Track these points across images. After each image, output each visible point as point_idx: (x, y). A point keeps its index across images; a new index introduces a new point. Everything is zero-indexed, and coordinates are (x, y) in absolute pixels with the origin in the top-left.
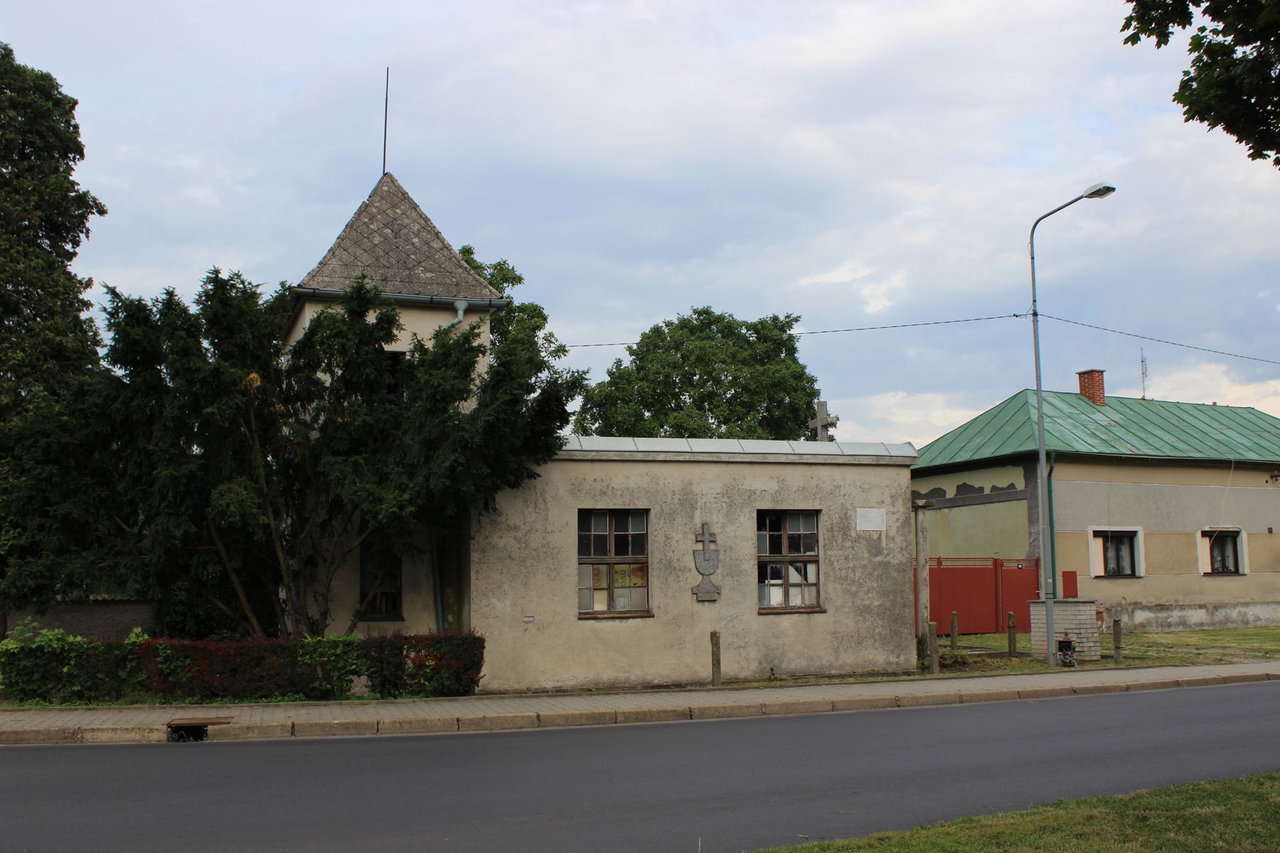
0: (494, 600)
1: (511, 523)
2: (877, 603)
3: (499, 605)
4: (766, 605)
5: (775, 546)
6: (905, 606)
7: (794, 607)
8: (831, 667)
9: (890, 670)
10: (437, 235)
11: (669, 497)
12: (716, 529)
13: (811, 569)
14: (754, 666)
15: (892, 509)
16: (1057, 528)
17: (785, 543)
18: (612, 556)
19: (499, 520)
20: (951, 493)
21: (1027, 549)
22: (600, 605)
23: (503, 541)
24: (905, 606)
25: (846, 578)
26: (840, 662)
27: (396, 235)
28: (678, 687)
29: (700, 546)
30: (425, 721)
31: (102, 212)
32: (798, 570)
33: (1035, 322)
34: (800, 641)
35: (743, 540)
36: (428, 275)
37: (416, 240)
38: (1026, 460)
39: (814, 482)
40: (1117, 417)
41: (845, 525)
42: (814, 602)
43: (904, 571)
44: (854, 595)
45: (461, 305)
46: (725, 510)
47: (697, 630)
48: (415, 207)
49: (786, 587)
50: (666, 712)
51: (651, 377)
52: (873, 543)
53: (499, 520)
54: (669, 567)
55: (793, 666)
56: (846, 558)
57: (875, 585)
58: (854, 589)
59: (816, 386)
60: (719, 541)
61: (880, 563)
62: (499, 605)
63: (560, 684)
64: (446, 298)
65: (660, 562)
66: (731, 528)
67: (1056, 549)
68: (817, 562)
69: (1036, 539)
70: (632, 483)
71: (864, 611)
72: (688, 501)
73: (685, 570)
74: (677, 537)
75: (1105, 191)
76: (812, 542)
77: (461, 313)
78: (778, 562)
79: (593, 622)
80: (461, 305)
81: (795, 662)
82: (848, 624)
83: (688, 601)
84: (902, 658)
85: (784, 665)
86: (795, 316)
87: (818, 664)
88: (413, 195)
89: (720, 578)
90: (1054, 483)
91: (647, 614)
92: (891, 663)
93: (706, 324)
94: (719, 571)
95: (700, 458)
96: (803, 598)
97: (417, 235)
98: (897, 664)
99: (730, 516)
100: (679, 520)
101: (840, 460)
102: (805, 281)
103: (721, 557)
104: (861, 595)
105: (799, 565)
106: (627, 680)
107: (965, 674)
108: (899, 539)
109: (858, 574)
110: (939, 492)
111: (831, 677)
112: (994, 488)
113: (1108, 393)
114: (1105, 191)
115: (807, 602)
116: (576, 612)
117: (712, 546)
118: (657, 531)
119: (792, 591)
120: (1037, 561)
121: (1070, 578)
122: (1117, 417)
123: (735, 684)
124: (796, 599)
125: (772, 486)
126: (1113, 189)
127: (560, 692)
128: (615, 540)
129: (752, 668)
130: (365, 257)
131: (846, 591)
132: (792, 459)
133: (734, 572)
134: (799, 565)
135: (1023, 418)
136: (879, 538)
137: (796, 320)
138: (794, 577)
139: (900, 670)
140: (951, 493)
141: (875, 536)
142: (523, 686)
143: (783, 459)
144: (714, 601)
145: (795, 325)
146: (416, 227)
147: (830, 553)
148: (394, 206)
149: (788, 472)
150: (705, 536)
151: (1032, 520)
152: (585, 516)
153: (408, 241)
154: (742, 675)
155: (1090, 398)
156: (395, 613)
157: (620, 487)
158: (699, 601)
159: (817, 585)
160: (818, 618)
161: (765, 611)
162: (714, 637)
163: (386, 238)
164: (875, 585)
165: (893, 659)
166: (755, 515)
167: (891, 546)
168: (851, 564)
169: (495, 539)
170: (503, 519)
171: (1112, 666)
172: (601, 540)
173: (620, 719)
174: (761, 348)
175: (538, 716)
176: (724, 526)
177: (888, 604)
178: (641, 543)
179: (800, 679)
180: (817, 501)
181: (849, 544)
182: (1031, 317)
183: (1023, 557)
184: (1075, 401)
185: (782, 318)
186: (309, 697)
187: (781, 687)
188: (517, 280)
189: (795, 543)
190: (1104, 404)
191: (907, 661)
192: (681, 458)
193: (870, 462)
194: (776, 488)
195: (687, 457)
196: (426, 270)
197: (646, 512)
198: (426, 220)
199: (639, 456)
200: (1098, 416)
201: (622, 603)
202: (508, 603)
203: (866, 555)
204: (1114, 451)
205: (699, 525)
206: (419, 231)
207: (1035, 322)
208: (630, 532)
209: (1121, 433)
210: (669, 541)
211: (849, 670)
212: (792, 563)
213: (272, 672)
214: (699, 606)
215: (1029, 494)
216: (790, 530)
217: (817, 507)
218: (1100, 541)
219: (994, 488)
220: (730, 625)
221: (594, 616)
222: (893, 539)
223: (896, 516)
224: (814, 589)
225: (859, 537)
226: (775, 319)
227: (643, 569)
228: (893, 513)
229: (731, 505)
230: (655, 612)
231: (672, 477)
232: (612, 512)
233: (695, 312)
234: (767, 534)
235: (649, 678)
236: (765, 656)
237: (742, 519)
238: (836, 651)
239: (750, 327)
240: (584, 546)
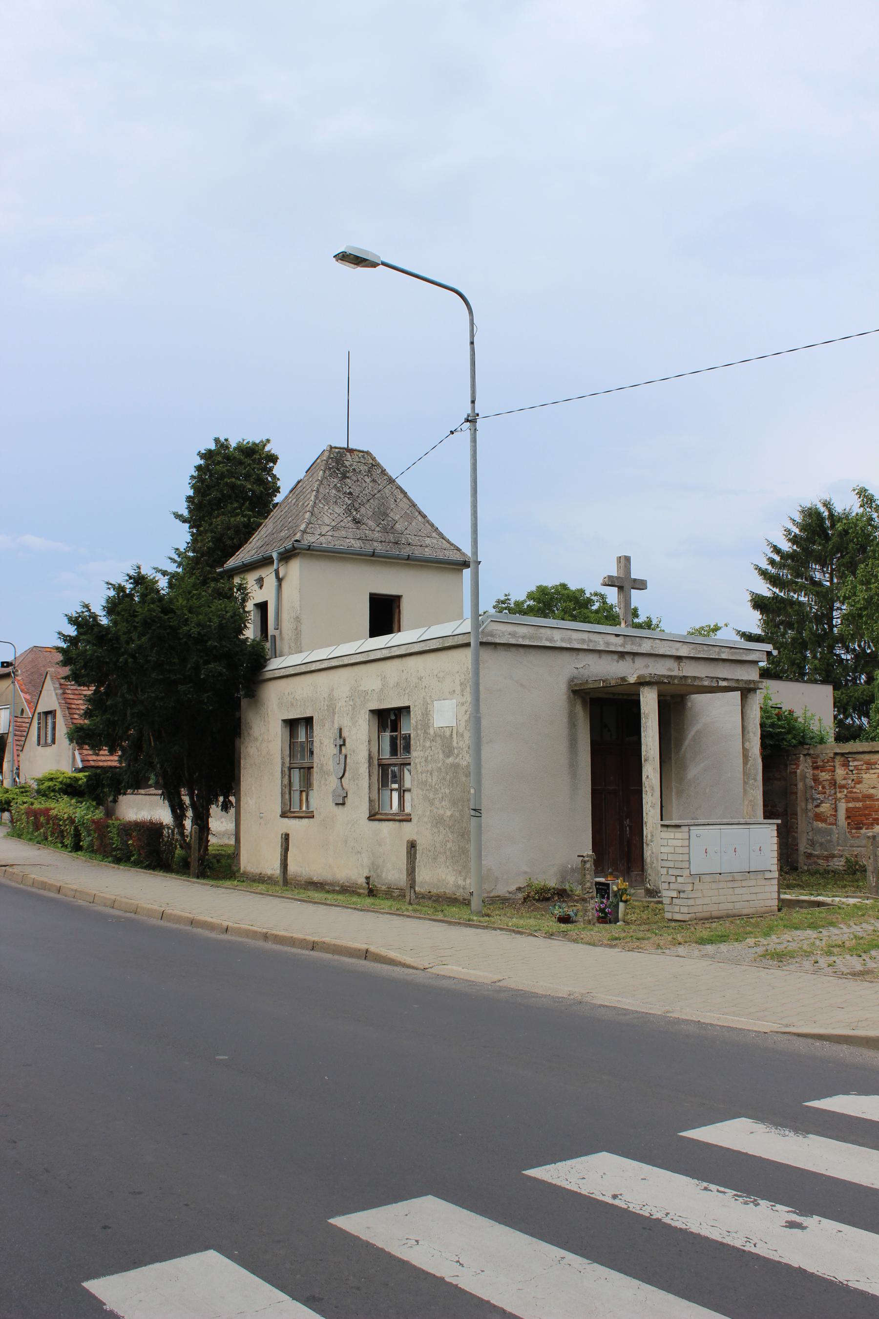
2: (449, 813)
92: (458, 887)
123: (317, 888)
141: (448, 734)
167: (461, 744)
168: (429, 768)
177: (457, 814)
197: (409, 707)
203: (441, 756)
228: (463, 704)
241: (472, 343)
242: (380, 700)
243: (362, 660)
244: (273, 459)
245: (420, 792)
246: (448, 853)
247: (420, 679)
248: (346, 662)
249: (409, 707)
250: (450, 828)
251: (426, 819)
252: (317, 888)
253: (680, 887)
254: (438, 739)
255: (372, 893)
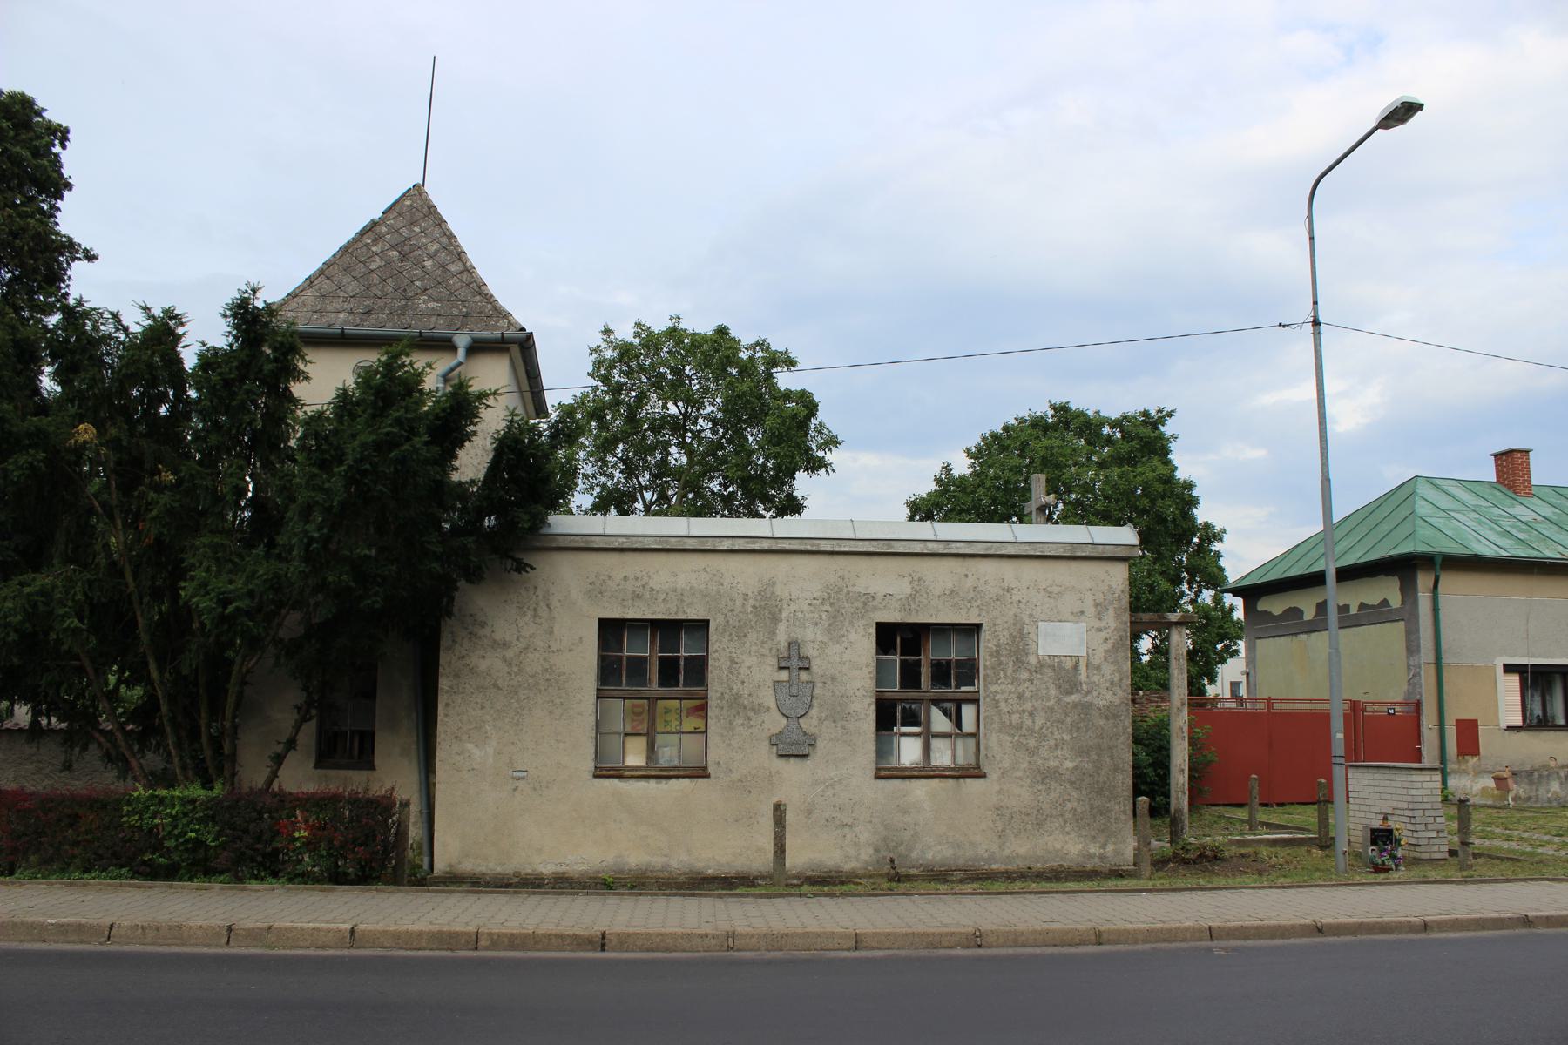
0: (469, 746)
1: (498, 636)
2: (1069, 765)
3: (477, 753)
4: (893, 762)
5: (910, 676)
6: (1116, 769)
7: (937, 768)
8: (992, 859)
9: (1089, 867)
10: (460, 255)
11: (739, 603)
12: (810, 651)
13: (968, 712)
14: (866, 854)
15: (1097, 624)
16: (1447, 660)
17: (926, 673)
18: (654, 686)
19: (481, 632)
20: (1309, 614)
21: (1405, 687)
22: (635, 756)
23: (488, 663)
24: (1116, 769)
25: (1020, 727)
26: (1007, 852)
27: (404, 257)
28: (698, 884)
29: (784, 675)
30: (180, 927)
31: (90, 257)
32: (945, 712)
33: (1317, 335)
34: (941, 821)
35: (854, 666)
36: (431, 305)
37: (428, 263)
38: (1404, 567)
39: (970, 583)
40: (1548, 511)
41: (1019, 645)
42: (972, 761)
43: (1116, 717)
44: (1032, 752)
45: (462, 341)
46: (825, 623)
47: (798, 794)
48: (441, 222)
49: (927, 737)
50: (561, 936)
51: (988, 483)
52: (1066, 675)
53: (481, 632)
54: (736, 704)
55: (930, 856)
56: (1020, 697)
57: (1066, 737)
58: (1032, 742)
59: (1195, 493)
60: (815, 669)
61: (1075, 705)
62: (477, 753)
63: (564, 869)
64: (442, 331)
65: (722, 697)
66: (834, 650)
67: (1446, 688)
68: (976, 701)
69: (1417, 675)
70: (681, 583)
71: (1047, 776)
72: (768, 610)
73: (759, 709)
74: (749, 661)
75: (1403, 112)
76: (968, 671)
77: (461, 352)
78: (914, 701)
79: (616, 781)
80: (462, 341)
81: (933, 850)
82: (1021, 794)
83: (764, 757)
84: (1110, 848)
85: (914, 854)
86: (1168, 409)
87: (970, 853)
88: (443, 211)
89: (815, 722)
90: (1442, 598)
91: (701, 772)
92: (1091, 856)
93: (1066, 419)
94: (813, 712)
95: (787, 546)
96: (954, 756)
97: (431, 257)
98: (1102, 857)
99: (834, 629)
100: (753, 636)
101: (1012, 550)
102: (1268, 399)
103: (817, 691)
104: (1044, 752)
105: (947, 705)
106: (665, 868)
107: (1222, 882)
108: (1108, 669)
109: (1040, 721)
110: (1295, 612)
111: (991, 876)
112: (1362, 606)
113: (1536, 479)
114: (1403, 112)
115: (961, 761)
116: (591, 765)
117: (804, 676)
118: (720, 649)
119: (936, 744)
120: (1418, 704)
121: (1468, 734)
122: (1548, 511)
123: (825, 882)
124: (942, 755)
125: (903, 588)
126: (1420, 107)
127: (563, 884)
128: (656, 662)
129: (864, 856)
130: (353, 287)
131: (1018, 746)
132: (932, 547)
133: (839, 713)
134: (947, 705)
135: (1403, 512)
136: (1076, 667)
137: (1170, 415)
138: (940, 722)
139: (1106, 867)
140: (1309, 614)
141: (1069, 664)
142: (507, 868)
143: (918, 548)
144: (805, 756)
145: (1169, 421)
146: (434, 247)
147: (993, 688)
148: (413, 223)
149: (927, 567)
150: (794, 660)
151: (1412, 648)
152: (611, 630)
153: (418, 264)
154: (847, 867)
155: (1509, 488)
156: (364, 758)
157: (666, 589)
158: (781, 756)
159: (975, 735)
160: (971, 785)
161: (886, 772)
162: (779, 811)
163: (389, 262)
164: (1066, 737)
165: (1094, 849)
166: (873, 631)
167: (1096, 679)
168: (1028, 706)
169: (474, 660)
170: (486, 631)
171: (1458, 876)
172: (637, 668)
173: (483, 943)
174: (1125, 448)
175: (352, 931)
176: (823, 646)
177: (1089, 766)
178: (698, 669)
179: (939, 878)
180: (975, 611)
181: (1024, 675)
182: (1309, 328)
183: (1399, 699)
184: (1486, 492)
185: (1153, 413)
186: (137, 874)
187: (843, 895)
188: (790, 363)
189: (942, 673)
190: (1530, 495)
191: (1117, 853)
192: (756, 547)
193: (1060, 552)
194: (908, 590)
195: (766, 545)
196: (431, 299)
197: (703, 625)
198: (452, 237)
199: (691, 544)
200: (1519, 511)
201: (668, 755)
202: (490, 750)
203: (1053, 692)
204: (1534, 554)
205: (784, 644)
206: (437, 252)
207: (1317, 335)
208: (683, 653)
209: (1550, 531)
210: (740, 666)
211: (1020, 864)
212: (936, 702)
213: (89, 837)
214: (781, 763)
215: (1408, 615)
216: (933, 653)
217: (973, 619)
218: (1515, 680)
219: (1362, 606)
220: (830, 792)
221: (619, 774)
222: (1098, 668)
223: (1103, 635)
224: (971, 742)
225: (1041, 665)
226: (1146, 414)
227: (702, 709)
228: (1099, 630)
229: (835, 616)
230: (711, 770)
231: (744, 574)
232: (656, 625)
233: (1053, 407)
234: (897, 658)
235: (699, 865)
236: (885, 839)
237: (852, 636)
238: (1001, 835)
239: (1115, 424)
240: (608, 671)
241: (1312, 238)
242: (902, 609)
243: (872, 550)
244: (69, 186)
245: (1006, 739)
246: (1068, 815)
247: (1009, 590)
248: (788, 547)
249: (708, 621)
250: (1072, 783)
251: (1019, 774)
252: (825, 882)
253: (1440, 827)
254: (1050, 672)
255: (897, 878)
